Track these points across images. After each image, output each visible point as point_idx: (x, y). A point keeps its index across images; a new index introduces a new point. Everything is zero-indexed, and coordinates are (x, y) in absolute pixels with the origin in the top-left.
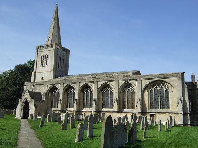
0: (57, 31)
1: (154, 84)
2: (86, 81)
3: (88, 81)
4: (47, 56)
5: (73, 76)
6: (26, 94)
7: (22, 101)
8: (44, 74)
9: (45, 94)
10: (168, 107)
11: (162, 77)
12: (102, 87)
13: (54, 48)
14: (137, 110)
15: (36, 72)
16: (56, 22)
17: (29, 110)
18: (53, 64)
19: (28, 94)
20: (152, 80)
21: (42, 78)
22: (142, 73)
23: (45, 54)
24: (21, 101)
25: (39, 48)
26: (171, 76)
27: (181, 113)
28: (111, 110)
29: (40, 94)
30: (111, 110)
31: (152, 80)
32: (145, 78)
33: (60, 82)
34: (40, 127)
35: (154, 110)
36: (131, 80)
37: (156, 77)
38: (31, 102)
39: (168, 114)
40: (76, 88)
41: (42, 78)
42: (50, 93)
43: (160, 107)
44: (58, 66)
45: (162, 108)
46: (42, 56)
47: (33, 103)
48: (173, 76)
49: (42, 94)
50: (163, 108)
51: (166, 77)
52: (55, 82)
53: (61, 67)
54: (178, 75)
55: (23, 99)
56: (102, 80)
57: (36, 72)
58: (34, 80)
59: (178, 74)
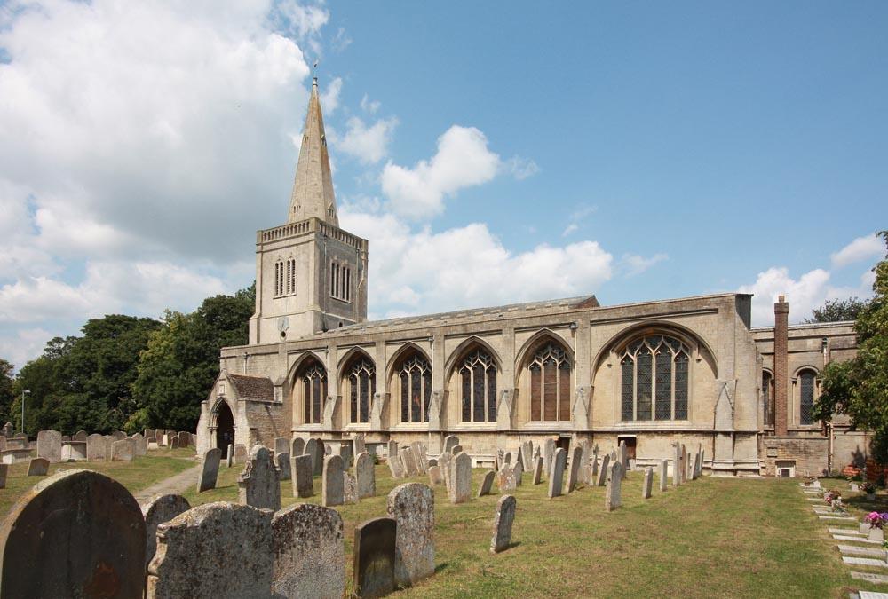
0: (320, 177)
1: (636, 337)
2: (408, 335)
3: (416, 336)
4: (294, 262)
5: (378, 324)
6: (219, 383)
7: (211, 406)
8: (287, 318)
9: (281, 383)
10: (682, 414)
11: (665, 311)
12: (462, 353)
13: (312, 236)
14: (574, 426)
15: (261, 315)
16: (315, 148)
17: (234, 431)
18: (312, 286)
19: (226, 383)
20: (630, 324)
21: (283, 334)
22: (603, 305)
23: (284, 255)
24: (208, 404)
25: (267, 235)
26: (698, 308)
27: (726, 434)
28: (492, 426)
29: (268, 380)
30: (421, 426)
31: (630, 324)
32: (606, 317)
33: (324, 344)
34: (198, 489)
35: (634, 425)
36: (555, 326)
37: (644, 314)
38: (237, 408)
39: (680, 435)
40: (382, 357)
41: (283, 334)
42: (299, 381)
43: (638, 416)
44: (330, 292)
45: (663, 414)
46: (277, 265)
47: (242, 409)
48: (705, 307)
49: (274, 380)
50: (667, 416)
51: (679, 310)
52: (310, 345)
53: (345, 300)
54: (722, 302)
55: (213, 399)
56: (460, 330)
57: (261, 315)
58: (258, 342)
59: (723, 299)
